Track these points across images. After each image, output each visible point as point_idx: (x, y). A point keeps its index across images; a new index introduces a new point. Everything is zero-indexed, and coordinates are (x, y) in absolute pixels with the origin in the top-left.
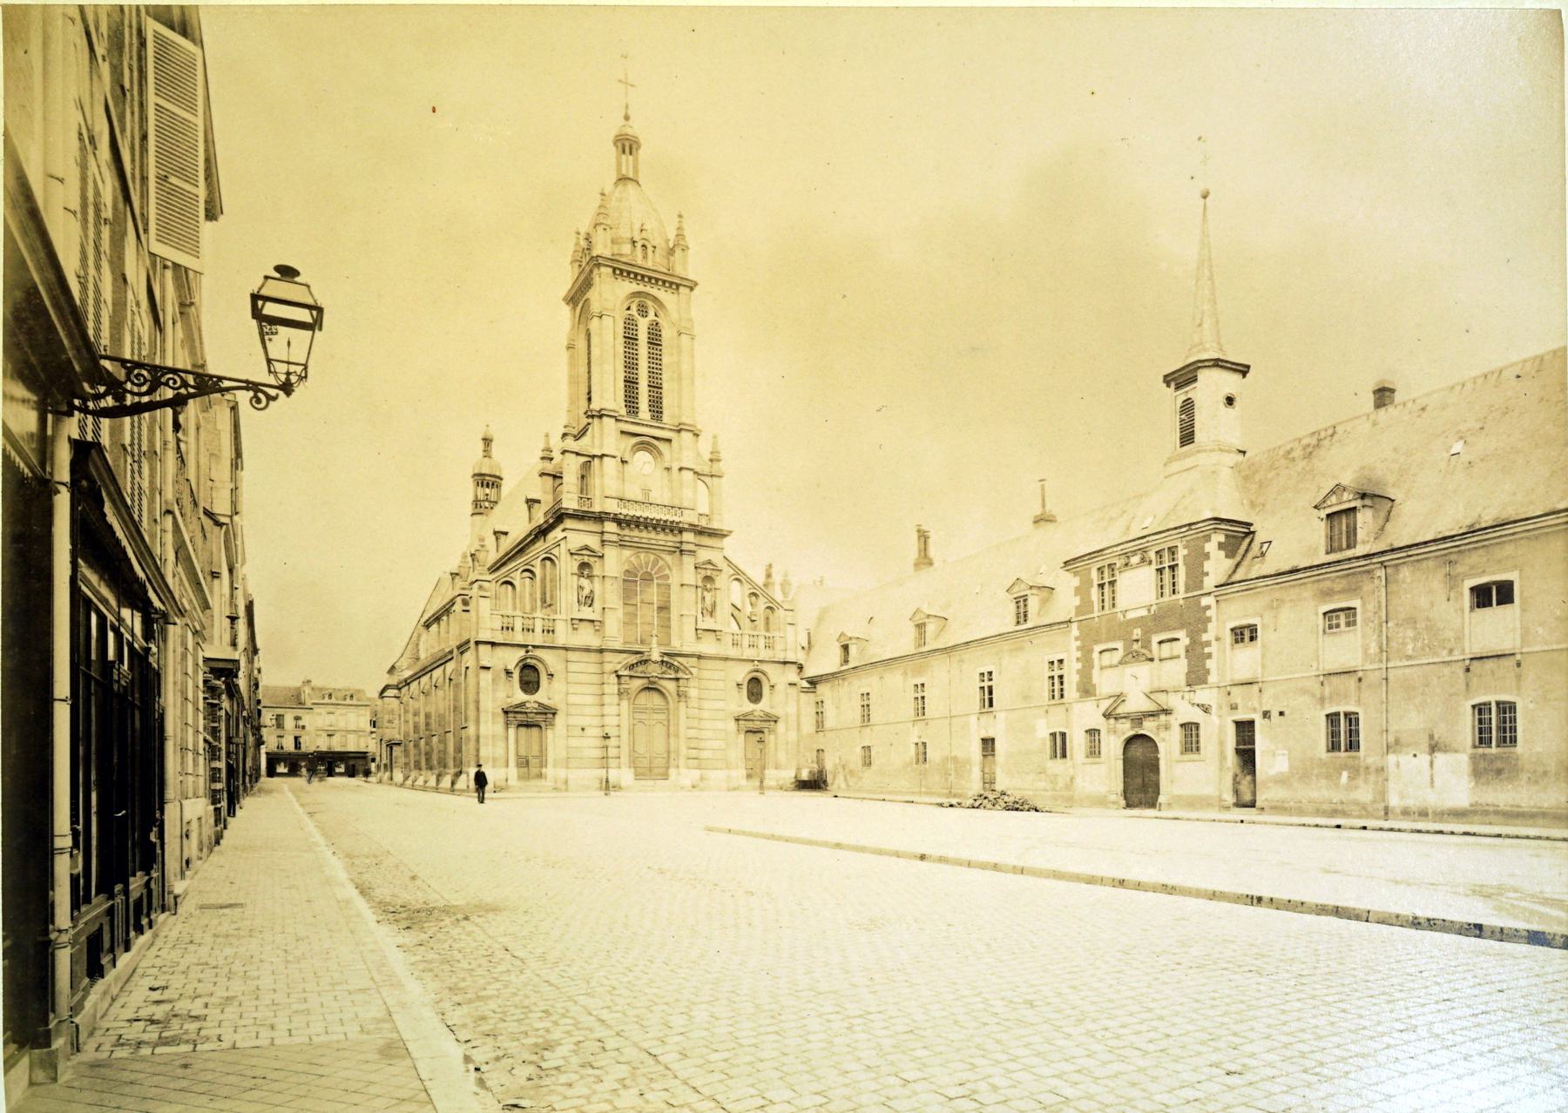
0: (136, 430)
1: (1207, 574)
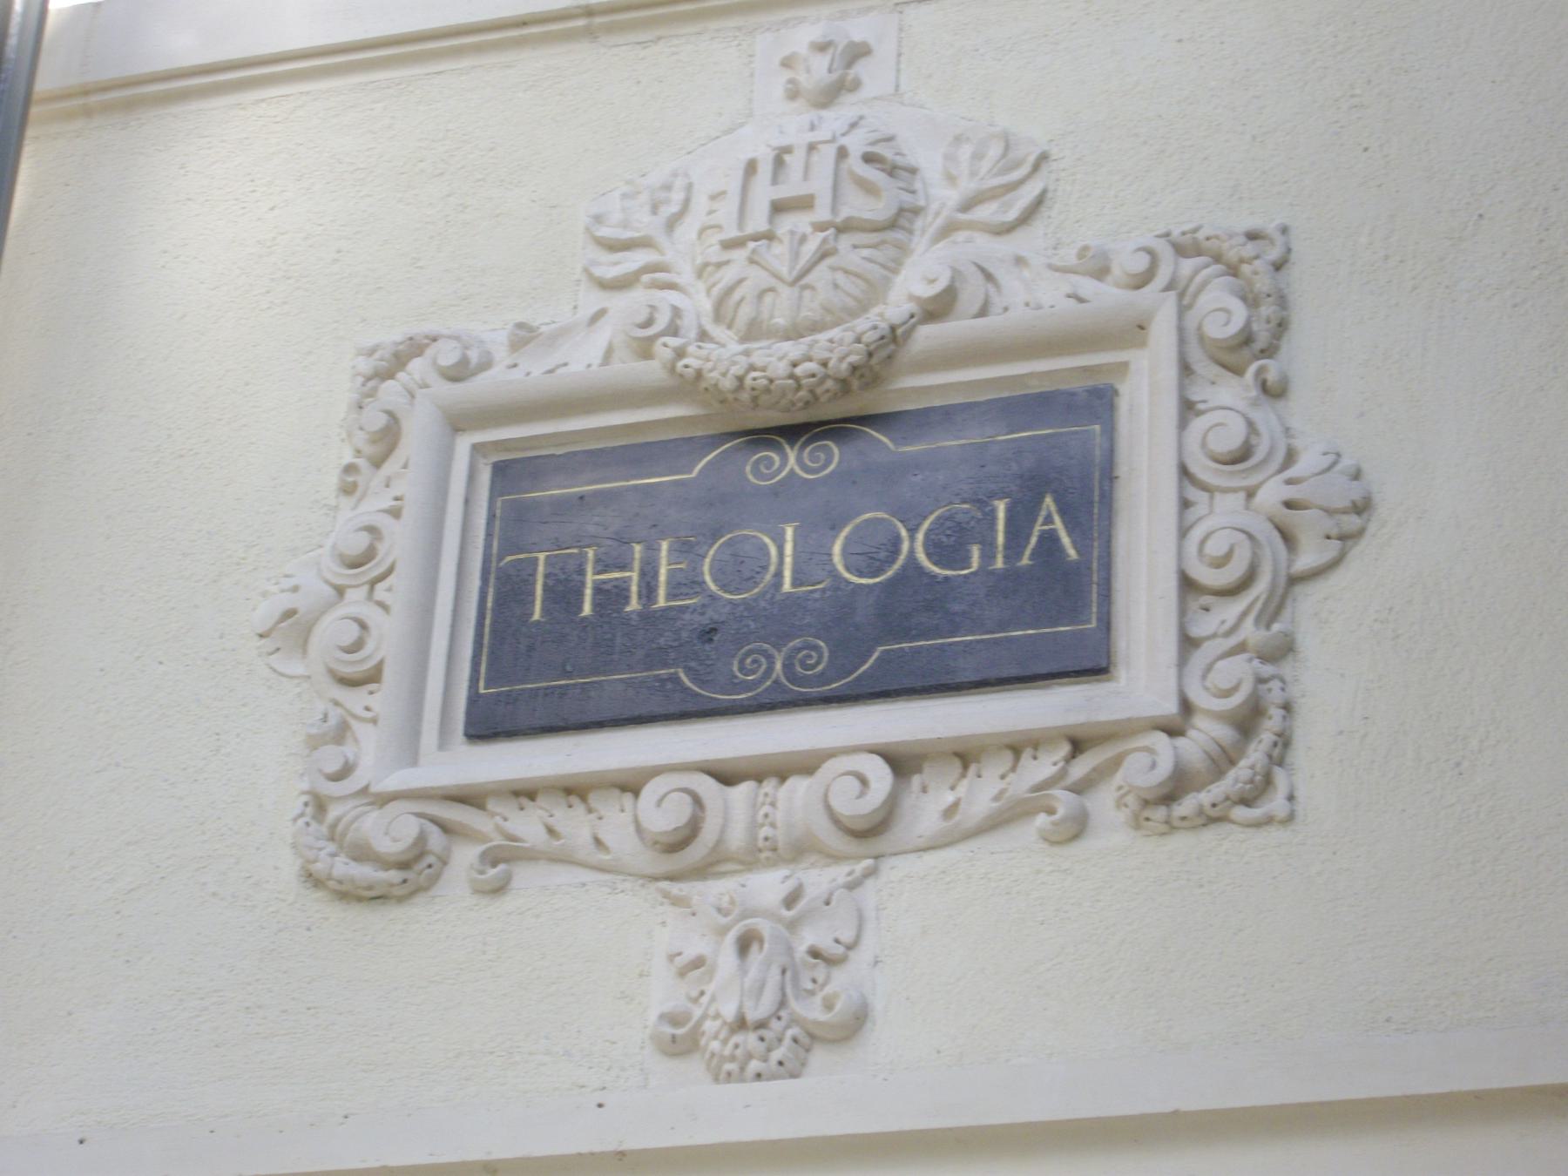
0: (581, 23)
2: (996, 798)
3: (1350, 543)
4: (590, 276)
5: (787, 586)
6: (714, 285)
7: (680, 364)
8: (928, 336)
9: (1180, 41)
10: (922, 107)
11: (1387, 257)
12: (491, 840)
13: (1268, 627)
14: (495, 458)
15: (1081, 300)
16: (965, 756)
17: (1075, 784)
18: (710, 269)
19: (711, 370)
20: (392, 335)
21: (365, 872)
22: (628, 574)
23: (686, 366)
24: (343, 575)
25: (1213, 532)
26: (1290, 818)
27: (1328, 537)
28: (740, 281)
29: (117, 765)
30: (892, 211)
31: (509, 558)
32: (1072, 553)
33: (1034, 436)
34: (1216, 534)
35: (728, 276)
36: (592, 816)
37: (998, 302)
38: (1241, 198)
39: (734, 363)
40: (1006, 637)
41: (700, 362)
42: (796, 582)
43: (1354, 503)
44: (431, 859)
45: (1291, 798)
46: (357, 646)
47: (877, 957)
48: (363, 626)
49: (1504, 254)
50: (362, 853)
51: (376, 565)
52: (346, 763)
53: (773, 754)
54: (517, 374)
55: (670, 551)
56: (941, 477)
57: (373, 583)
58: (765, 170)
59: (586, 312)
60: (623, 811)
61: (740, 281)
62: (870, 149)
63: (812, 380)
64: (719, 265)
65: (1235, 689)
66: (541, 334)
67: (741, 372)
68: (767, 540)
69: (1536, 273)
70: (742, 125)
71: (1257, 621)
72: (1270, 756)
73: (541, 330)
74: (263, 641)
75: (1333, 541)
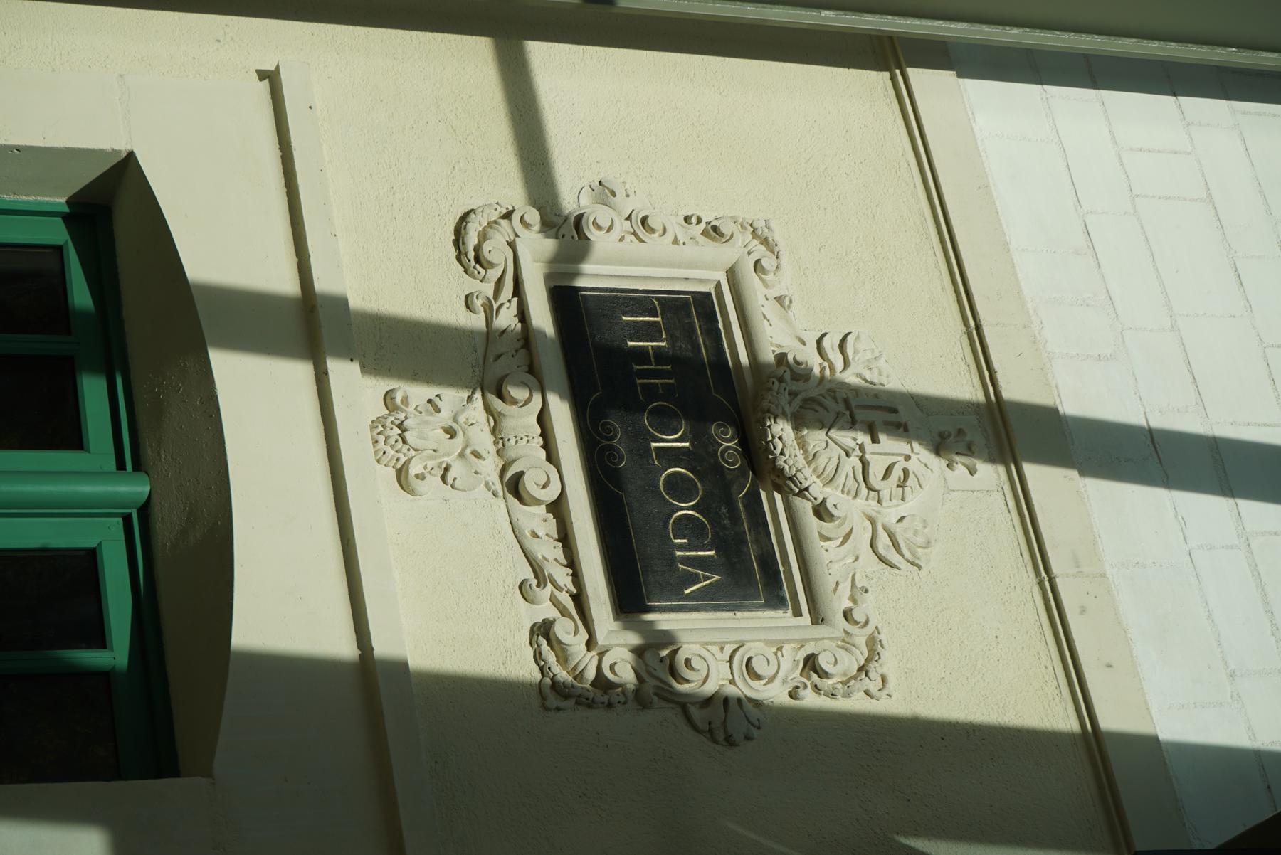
0: (972, 323)
1: (515, 316)
2: (544, 557)
3: (708, 736)
4: (824, 335)
5: (654, 444)
6: (823, 397)
7: (775, 380)
8: (805, 508)
9: (997, 637)
10: (943, 504)
11: (879, 751)
12: (495, 302)
13: (656, 694)
14: (713, 293)
15: (835, 590)
16: (565, 537)
17: (555, 597)
18: (832, 394)
19: (772, 395)
20: (777, 236)
21: (472, 240)
22: (653, 363)
23: (773, 383)
24: (637, 219)
25: (705, 660)
26: (547, 709)
27: (710, 723)
28: (826, 409)
29: (521, 116)
30: (877, 487)
31: (656, 302)
32: (687, 591)
33: (636, 316)
34: (724, 714)
35: (829, 403)
36: (514, 352)
37: (831, 545)
38: (906, 673)
39: (777, 406)
40: (636, 560)
41: (776, 389)
42: (657, 449)
43: (731, 736)
44: (482, 271)
45: (558, 709)
46: (599, 228)
47: (448, 500)
48: (609, 229)
49: (887, 813)
50: (483, 237)
51: (644, 234)
52: (531, 225)
53: (551, 418)
54: (761, 300)
55: (670, 384)
56: (725, 522)
57: (634, 233)
58: (892, 418)
59: (805, 336)
60: (518, 367)
61: (826, 409)
62: (911, 472)
63: (772, 448)
64: (835, 398)
65: (615, 674)
66: (787, 312)
67: (772, 410)
68: (680, 434)
69: (878, 831)
70: (922, 411)
71: (658, 687)
72: (579, 696)
73: (789, 312)
74: (598, 183)
75: (708, 726)
